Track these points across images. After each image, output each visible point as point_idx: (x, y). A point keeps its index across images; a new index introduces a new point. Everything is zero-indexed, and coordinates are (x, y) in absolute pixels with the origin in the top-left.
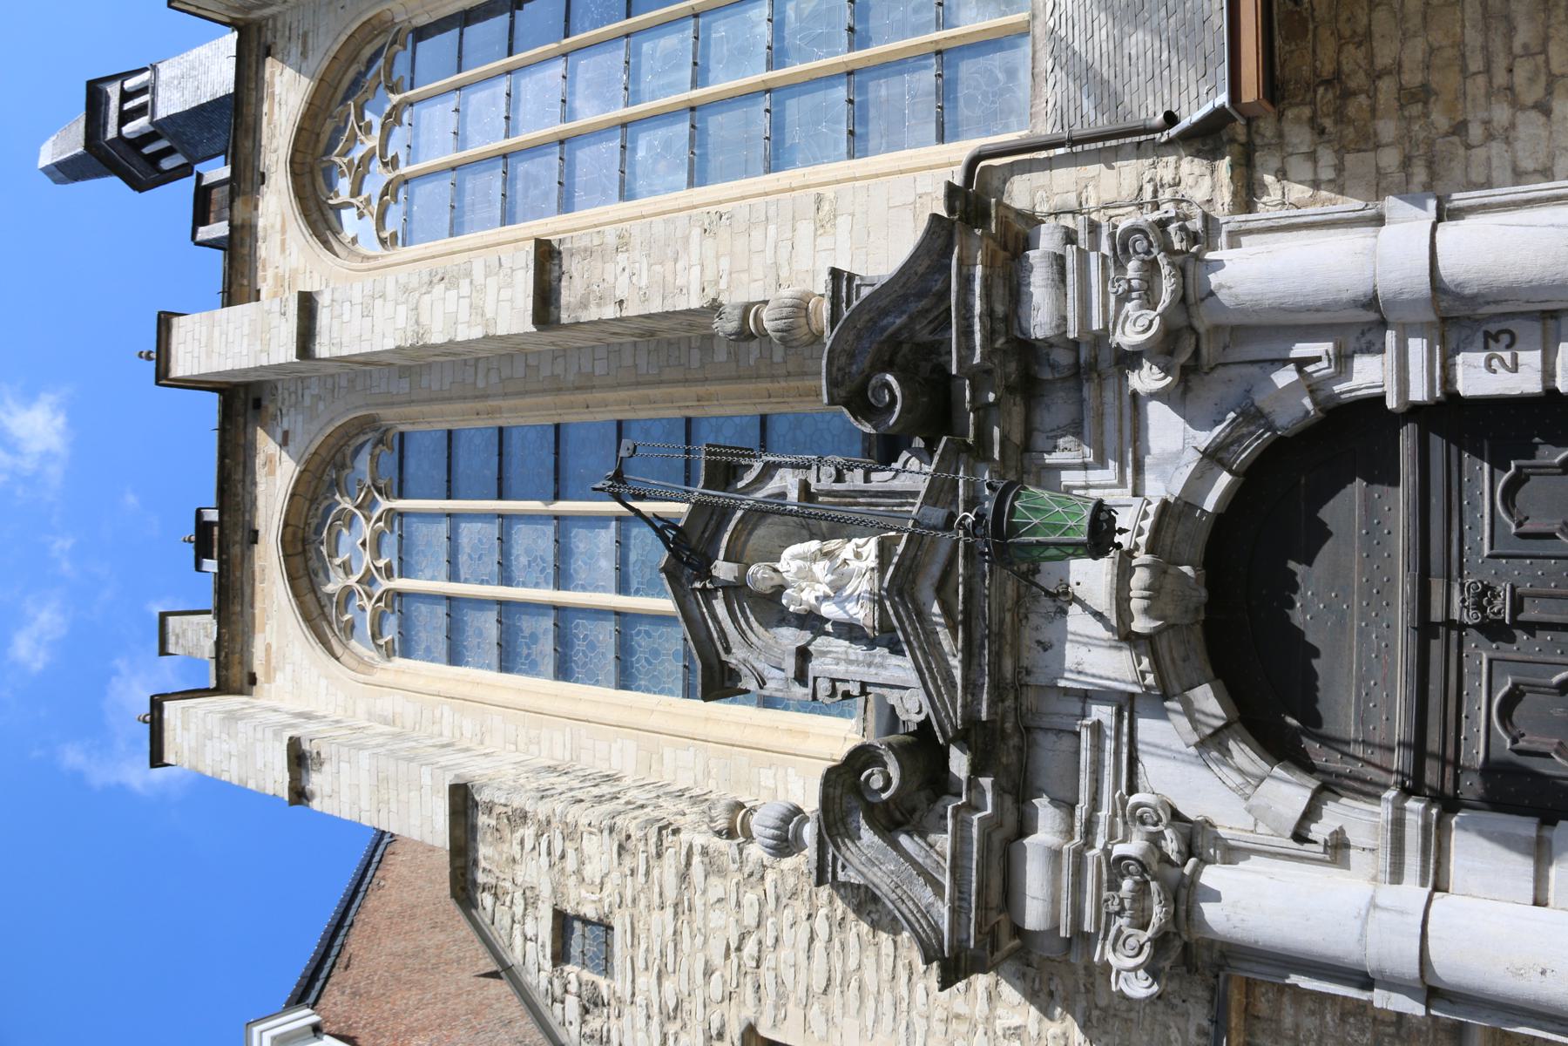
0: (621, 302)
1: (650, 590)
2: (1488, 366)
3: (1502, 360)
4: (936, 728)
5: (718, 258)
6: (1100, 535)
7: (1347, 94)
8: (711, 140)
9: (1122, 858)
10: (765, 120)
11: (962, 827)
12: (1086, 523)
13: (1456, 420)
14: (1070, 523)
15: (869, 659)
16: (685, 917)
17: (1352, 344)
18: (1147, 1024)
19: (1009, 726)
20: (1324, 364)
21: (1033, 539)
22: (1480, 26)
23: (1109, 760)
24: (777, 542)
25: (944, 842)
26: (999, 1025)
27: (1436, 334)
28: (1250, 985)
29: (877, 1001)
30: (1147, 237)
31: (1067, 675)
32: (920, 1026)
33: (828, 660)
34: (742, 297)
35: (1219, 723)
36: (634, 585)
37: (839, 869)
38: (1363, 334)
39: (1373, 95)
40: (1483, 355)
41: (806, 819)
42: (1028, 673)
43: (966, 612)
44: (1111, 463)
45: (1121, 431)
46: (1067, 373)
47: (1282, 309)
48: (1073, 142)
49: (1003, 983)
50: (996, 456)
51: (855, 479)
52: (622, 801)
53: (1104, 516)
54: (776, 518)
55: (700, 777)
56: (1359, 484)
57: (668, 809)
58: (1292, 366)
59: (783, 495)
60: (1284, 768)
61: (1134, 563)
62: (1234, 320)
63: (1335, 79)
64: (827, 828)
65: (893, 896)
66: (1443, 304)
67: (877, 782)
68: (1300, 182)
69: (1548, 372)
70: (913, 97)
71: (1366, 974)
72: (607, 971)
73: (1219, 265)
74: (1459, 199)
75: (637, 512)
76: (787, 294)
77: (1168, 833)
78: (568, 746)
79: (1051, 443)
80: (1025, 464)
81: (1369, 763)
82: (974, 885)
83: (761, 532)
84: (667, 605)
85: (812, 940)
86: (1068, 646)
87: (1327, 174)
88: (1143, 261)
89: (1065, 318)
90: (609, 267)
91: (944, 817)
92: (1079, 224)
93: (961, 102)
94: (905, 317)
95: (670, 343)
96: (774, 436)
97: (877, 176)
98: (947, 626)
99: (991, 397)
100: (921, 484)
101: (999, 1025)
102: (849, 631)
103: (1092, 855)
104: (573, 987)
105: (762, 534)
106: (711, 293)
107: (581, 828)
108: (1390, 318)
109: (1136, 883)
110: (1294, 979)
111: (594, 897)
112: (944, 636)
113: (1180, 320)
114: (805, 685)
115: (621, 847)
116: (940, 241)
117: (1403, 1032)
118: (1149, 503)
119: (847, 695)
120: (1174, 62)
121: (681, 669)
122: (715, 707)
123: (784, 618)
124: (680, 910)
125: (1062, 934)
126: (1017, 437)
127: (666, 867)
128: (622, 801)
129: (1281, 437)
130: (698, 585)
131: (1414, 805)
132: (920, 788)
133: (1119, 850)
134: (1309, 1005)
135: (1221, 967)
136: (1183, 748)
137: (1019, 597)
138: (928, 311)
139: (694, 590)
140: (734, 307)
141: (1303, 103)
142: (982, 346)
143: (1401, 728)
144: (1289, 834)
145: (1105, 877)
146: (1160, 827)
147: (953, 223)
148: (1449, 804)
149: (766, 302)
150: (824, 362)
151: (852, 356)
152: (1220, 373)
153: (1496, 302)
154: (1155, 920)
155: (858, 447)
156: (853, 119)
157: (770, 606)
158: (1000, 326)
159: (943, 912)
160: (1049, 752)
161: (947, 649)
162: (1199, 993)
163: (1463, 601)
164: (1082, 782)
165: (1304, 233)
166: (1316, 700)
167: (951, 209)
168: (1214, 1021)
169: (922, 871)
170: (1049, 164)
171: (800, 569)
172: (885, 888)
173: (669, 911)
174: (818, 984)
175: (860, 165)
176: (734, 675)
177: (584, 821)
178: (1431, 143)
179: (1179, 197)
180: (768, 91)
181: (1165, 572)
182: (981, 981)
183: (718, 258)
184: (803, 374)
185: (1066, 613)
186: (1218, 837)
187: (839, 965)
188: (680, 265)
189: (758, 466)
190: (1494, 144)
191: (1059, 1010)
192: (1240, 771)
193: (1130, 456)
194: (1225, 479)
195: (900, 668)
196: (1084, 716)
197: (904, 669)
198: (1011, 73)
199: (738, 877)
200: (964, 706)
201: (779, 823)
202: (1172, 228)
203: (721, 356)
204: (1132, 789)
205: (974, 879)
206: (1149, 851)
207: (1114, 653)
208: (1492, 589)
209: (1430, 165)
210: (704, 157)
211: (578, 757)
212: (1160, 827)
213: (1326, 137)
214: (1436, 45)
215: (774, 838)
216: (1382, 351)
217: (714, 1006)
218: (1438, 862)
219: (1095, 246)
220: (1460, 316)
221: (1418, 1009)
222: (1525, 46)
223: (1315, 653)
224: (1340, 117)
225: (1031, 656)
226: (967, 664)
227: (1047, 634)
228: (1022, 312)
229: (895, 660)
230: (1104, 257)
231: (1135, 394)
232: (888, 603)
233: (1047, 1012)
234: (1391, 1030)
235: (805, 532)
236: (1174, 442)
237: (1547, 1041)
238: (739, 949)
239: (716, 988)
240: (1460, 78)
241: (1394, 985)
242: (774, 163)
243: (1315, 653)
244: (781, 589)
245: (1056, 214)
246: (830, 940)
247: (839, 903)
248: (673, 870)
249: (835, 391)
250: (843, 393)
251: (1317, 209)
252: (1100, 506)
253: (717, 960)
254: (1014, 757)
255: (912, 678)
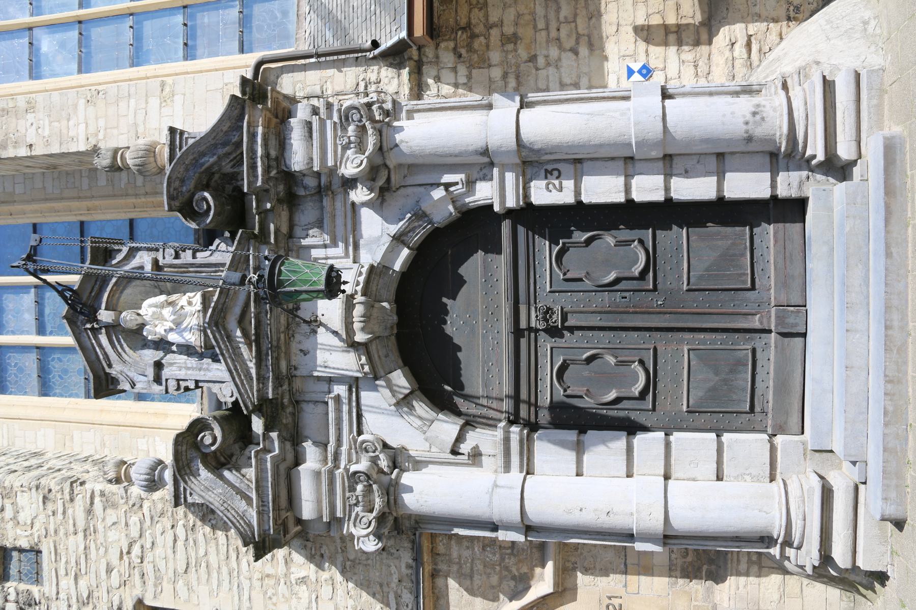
0: (31, 146)
1: (59, 332)
2: (547, 188)
3: (554, 185)
4: (242, 405)
5: (97, 119)
6: (332, 285)
7: (474, 36)
8: (93, 43)
9: (356, 473)
10: (129, 33)
11: (261, 463)
12: (323, 278)
13: (531, 217)
14: (314, 279)
15: (199, 366)
16: (92, 537)
17: (475, 175)
18: (378, 566)
19: (286, 401)
20: (460, 186)
21: (293, 289)
22: (543, 4)
23: (345, 417)
24: (139, 297)
25: (251, 473)
26: (293, 578)
27: (520, 170)
28: (433, 536)
29: (218, 573)
30: (359, 112)
31: (318, 369)
32: (246, 584)
33: (174, 368)
34: (113, 144)
35: (407, 391)
36: (49, 329)
37: (188, 495)
38: (481, 169)
39: (487, 38)
40: (544, 182)
41: (166, 467)
42: (296, 369)
43: (257, 334)
44: (340, 244)
45: (346, 225)
46: (313, 191)
47: (435, 155)
48: (318, 55)
49: (293, 552)
50: (272, 241)
51: (187, 257)
52: (45, 468)
53: (334, 274)
54: (138, 282)
55: (98, 448)
56: (480, 253)
57: (77, 470)
58: (442, 187)
59: (142, 268)
60: (445, 415)
61: (355, 301)
62: (410, 161)
63: (468, 27)
64: (179, 471)
65: (222, 508)
66: (523, 154)
67: (208, 440)
68: (448, 84)
69: (578, 192)
70: (225, 24)
71: (493, 523)
72: (38, 581)
73: (401, 129)
74: (532, 97)
75: (45, 281)
76: (142, 142)
77: (382, 456)
78: (6, 436)
79: (305, 233)
80: (289, 243)
81: (491, 408)
82: (270, 497)
83: (128, 291)
84: (69, 340)
85: (175, 541)
86: (318, 352)
87: (462, 80)
88: (357, 126)
89: (312, 159)
90: (22, 122)
91: (250, 458)
92: (319, 103)
93: (254, 29)
94: (215, 157)
95: (67, 173)
96: (138, 232)
97: (201, 72)
98: (246, 344)
99: (269, 206)
100: (227, 258)
101: (293, 578)
102: (187, 350)
103: (339, 472)
104: (12, 597)
105: (129, 293)
106: (93, 141)
107: (15, 489)
108: (495, 161)
109: (365, 486)
110: (456, 531)
111: (26, 533)
112: (244, 349)
113: (379, 161)
114: (161, 384)
115: (45, 498)
116: (236, 111)
117: (515, 551)
118: (363, 267)
119: (187, 389)
120: (378, 12)
121: (83, 380)
122: (104, 402)
123: (146, 344)
124: (88, 533)
125: (325, 520)
126: (284, 229)
127: (77, 507)
128: (45, 468)
129: (437, 228)
130: (88, 326)
131: (515, 429)
132: (235, 442)
133: (353, 468)
134: (465, 543)
135: (416, 529)
136: (388, 407)
137: (288, 324)
138: (230, 154)
139: (86, 329)
140: (107, 150)
141: (449, 39)
142: (263, 175)
143: (506, 388)
144: (449, 451)
145: (347, 484)
146: (377, 453)
147: (245, 101)
148: (533, 427)
149: (128, 148)
150: (165, 185)
151: (183, 181)
152: (402, 191)
153: (551, 153)
154: (377, 506)
155: (192, 238)
156: (186, 36)
157: (136, 337)
158: (274, 163)
159: (253, 515)
160: (310, 415)
161: (246, 357)
162: (406, 545)
163: (537, 316)
164: (331, 431)
165: (449, 112)
166: (460, 375)
167: (244, 92)
168: (415, 560)
169: (239, 492)
170: (304, 68)
171: (154, 313)
172: (216, 504)
173: (81, 535)
174: (181, 567)
175: (190, 65)
176: (115, 381)
177: (17, 484)
178: (518, 66)
179: (379, 90)
180: (131, 14)
181: (373, 306)
182: (280, 553)
183: (97, 119)
184: (157, 193)
185: (316, 332)
186: (410, 456)
187: (193, 555)
188: (71, 123)
189: (125, 250)
190: (550, 68)
191: (327, 564)
192: (420, 418)
193: (351, 240)
194: (405, 252)
195: (218, 370)
196: (330, 392)
197: (221, 370)
198: (285, 13)
199: (125, 507)
200: (258, 391)
201: (149, 471)
202: (374, 107)
203: (102, 181)
204: (360, 433)
205: (270, 493)
206: (371, 468)
207: (345, 354)
208: (551, 309)
209: (517, 77)
210: (89, 54)
211: (13, 444)
212: (377, 453)
213: (462, 59)
214: (521, 12)
215: (146, 480)
216: (491, 179)
217: (115, 591)
218: (528, 459)
219: (330, 117)
220: (533, 161)
221: (519, 538)
222: (566, 18)
223: (459, 349)
224: (470, 49)
225: (297, 359)
226: (259, 366)
227: (306, 346)
228: (286, 155)
229: (215, 366)
230: (335, 123)
231: (353, 204)
232: (209, 331)
233: (320, 566)
234: (509, 551)
235: (157, 290)
236: (377, 231)
237: (584, 544)
238: (129, 553)
239: (115, 580)
240: (533, 31)
241: (509, 527)
242: (136, 60)
243: (459, 349)
244: (142, 326)
245: (308, 98)
246: (187, 540)
247: (191, 517)
248: (82, 508)
249: (172, 203)
250: (177, 204)
251: (457, 99)
252: (331, 268)
253: (115, 561)
254: (290, 419)
255: (226, 376)
